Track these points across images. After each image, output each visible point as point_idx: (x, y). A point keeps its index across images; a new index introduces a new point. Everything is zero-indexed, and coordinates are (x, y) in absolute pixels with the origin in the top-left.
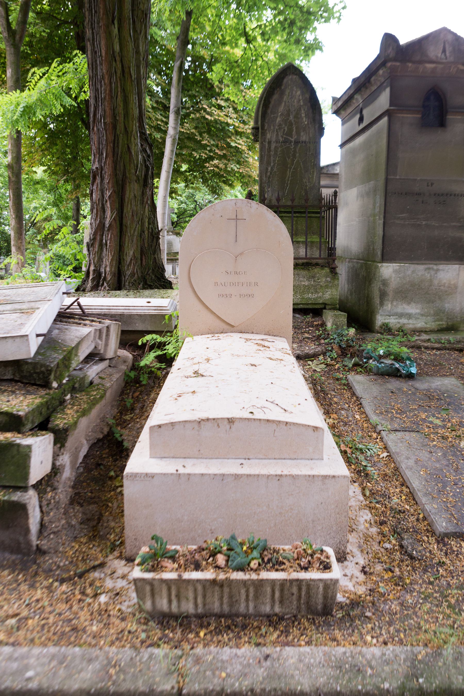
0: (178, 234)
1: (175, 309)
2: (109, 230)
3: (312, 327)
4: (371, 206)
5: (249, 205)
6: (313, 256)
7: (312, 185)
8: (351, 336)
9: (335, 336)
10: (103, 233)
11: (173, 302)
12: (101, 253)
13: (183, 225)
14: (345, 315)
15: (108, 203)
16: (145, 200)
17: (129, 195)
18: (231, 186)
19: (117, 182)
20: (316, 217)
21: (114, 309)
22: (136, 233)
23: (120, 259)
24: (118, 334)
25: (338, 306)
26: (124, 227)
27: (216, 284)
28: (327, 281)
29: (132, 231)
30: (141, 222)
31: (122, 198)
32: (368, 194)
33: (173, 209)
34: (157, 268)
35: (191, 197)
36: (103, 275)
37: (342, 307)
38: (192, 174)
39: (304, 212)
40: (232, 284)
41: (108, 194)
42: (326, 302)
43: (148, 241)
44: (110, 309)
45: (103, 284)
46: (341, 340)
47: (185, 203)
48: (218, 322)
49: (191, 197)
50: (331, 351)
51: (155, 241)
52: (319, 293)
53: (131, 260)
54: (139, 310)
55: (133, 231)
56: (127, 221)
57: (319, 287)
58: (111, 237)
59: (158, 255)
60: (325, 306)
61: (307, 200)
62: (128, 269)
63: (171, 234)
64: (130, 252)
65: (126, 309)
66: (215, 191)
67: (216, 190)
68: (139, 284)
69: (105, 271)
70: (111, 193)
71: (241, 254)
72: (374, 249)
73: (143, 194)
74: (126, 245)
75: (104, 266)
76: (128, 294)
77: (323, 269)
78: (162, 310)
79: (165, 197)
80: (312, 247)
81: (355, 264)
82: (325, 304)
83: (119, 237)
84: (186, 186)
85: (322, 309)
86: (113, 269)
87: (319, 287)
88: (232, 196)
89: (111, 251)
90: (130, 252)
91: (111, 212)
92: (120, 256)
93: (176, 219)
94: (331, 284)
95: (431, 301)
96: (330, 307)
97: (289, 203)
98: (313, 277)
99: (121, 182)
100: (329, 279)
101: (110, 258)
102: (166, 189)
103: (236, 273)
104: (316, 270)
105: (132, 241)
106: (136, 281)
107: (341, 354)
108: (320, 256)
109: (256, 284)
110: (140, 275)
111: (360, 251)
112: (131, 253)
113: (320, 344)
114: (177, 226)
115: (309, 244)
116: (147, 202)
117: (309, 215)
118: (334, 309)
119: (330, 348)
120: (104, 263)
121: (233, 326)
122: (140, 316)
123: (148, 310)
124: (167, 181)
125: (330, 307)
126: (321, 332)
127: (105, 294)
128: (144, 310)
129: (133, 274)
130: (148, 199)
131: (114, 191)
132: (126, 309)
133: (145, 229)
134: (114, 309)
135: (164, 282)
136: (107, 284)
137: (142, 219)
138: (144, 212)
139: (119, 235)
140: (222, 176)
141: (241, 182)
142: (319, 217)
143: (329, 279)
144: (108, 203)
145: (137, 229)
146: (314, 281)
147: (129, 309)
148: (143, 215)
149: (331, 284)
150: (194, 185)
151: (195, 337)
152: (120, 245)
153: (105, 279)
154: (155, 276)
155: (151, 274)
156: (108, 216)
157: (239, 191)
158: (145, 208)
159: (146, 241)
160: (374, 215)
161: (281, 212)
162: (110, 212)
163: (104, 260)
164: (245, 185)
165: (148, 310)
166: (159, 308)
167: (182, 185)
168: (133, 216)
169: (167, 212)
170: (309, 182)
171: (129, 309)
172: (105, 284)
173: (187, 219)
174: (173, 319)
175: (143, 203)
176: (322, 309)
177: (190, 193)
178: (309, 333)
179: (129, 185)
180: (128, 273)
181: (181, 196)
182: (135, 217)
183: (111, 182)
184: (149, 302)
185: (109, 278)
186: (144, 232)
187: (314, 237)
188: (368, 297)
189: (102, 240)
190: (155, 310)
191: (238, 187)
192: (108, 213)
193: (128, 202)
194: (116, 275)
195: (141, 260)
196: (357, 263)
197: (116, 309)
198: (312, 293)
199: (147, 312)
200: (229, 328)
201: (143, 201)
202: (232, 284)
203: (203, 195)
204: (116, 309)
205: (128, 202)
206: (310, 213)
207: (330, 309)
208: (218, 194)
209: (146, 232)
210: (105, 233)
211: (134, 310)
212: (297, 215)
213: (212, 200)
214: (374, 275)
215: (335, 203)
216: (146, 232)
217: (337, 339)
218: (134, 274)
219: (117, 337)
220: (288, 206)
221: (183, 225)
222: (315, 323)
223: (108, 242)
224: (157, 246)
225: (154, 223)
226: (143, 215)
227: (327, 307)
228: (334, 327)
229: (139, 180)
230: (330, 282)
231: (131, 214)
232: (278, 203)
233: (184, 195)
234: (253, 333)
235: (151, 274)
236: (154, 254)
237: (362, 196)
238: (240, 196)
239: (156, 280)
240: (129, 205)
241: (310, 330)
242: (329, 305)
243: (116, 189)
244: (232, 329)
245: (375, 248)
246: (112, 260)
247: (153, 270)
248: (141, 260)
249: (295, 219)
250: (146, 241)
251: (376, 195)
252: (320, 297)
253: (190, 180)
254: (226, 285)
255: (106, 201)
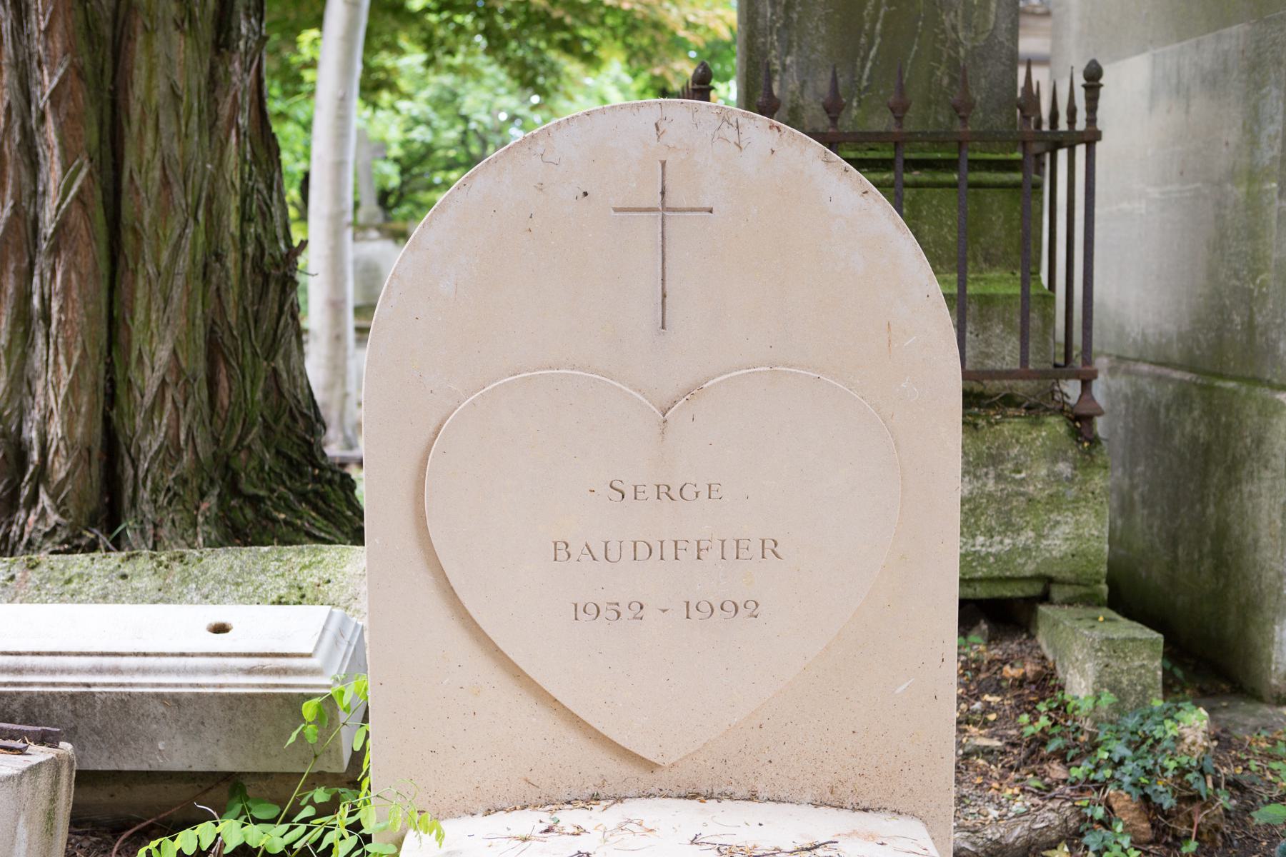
0: (400, 236)
1: (357, 664)
2: (55, 250)
3: (998, 690)
4: (1233, 135)
5: (730, 133)
6: (991, 364)
7: (981, 41)
8: (1198, 751)
9: (1120, 750)
10: (32, 264)
11: (345, 620)
12: (25, 356)
13: (423, 197)
14: (1153, 643)
15: (50, 125)
16: (225, 110)
17: (149, 89)
18: (590, 60)
19: (90, 29)
20: (1003, 186)
21: (42, 671)
22: (183, 263)
23: (112, 383)
24: (50, 816)
25: (1104, 588)
26: (128, 238)
27: (562, 550)
28: (1056, 478)
29: (165, 256)
30: (209, 211)
31: (114, 104)
32: (1213, 81)
33: (383, 146)
34: (285, 418)
35: (446, 101)
36: (35, 456)
37: (1125, 596)
38: (449, 20)
39: (950, 165)
40: (642, 550)
41: (47, 81)
42: (1053, 572)
43: (242, 296)
44: (19, 671)
45: (33, 499)
46: (1149, 773)
47: (428, 123)
48: (574, 747)
49: (446, 101)
50: (1106, 824)
51: (273, 292)
52: (1018, 531)
53: (163, 383)
54: (169, 671)
55: (167, 249)
56: (142, 207)
57: (1018, 502)
58: (66, 281)
59: (287, 358)
60: (1045, 588)
61: (962, 110)
62: (149, 427)
63: (374, 234)
64: (158, 351)
65: (100, 671)
66: (528, 77)
67: (536, 75)
68: (203, 495)
69: (43, 437)
70: (62, 81)
71: (692, 392)
72: (1250, 327)
73: (213, 82)
74: (140, 316)
75: (36, 415)
76: (127, 569)
77: (1037, 423)
78: (284, 671)
79: (343, 101)
80: (984, 320)
81: (1145, 383)
82: (1048, 581)
83: (104, 284)
84: (430, 63)
85: (1031, 603)
86: (79, 430)
87: (1018, 502)
88: (589, 96)
89: (67, 345)
90: (158, 351)
91: (65, 169)
92: (110, 368)
93: (394, 181)
94: (1073, 492)
95: (310, 445)
96: (1068, 591)
97: (881, 122)
98: (995, 459)
99: (107, 31)
100: (1064, 468)
101: (66, 378)
102: (346, 70)
103: (664, 491)
104: (1006, 429)
105: (167, 300)
106: (185, 482)
107: (1149, 836)
108: (1024, 361)
109: (770, 548)
110: (205, 450)
111: (1170, 328)
112: (163, 354)
113: (1045, 792)
114: (394, 206)
115: (972, 309)
116: (232, 120)
117: (973, 177)
118: (1089, 600)
119: (1100, 813)
120: (40, 399)
121: (651, 766)
122: (175, 701)
123: (215, 672)
124: (348, 38)
125: (1068, 591)
126: (1044, 721)
127: (17, 571)
128: (196, 671)
129: (171, 451)
130: (236, 107)
131: (77, 71)
132: (100, 671)
133: (228, 244)
134: (42, 671)
135: (317, 479)
136: (53, 497)
137: (210, 199)
138: (220, 165)
139: (104, 268)
140: (559, 25)
141: (628, 46)
142: (1016, 186)
143: (1064, 468)
144: (50, 125)
145: (186, 244)
146: (999, 478)
147: (116, 671)
148: (213, 182)
149: (1073, 492)
150: (458, 60)
151: (449, 826)
152: (112, 322)
153: (42, 473)
154: (278, 453)
155: (257, 447)
156: (52, 187)
157: (617, 81)
158: (224, 145)
159: (231, 298)
160: (1254, 176)
161: (885, 165)
162: (57, 167)
163: (39, 386)
164: (638, 57)
165: (215, 672)
166: (268, 662)
167: (414, 58)
168: (166, 183)
169: (351, 157)
170: (968, 26)
171: (116, 671)
172: (44, 499)
173: (438, 178)
174: (343, 717)
175: (213, 126)
176: (1031, 603)
177: (444, 88)
178: (986, 723)
179: (148, 44)
180: (152, 444)
181: (409, 97)
182: (177, 189)
183: (59, 26)
184: (220, 629)
185: (60, 469)
186: (219, 257)
187: (994, 274)
188: (1222, 533)
189: (29, 296)
190: (250, 671)
191: (615, 64)
192: (52, 173)
193: (143, 121)
194: (96, 453)
195: (212, 383)
196: (1159, 378)
197: (53, 671)
198: (990, 532)
199: (209, 683)
200: (633, 775)
201: (215, 118)
202: (642, 550)
203: (489, 95)
204: (53, 671)
205: (143, 121)
206: (975, 165)
207: (1070, 602)
208: (542, 91)
209: (231, 259)
210: (42, 262)
211: (145, 671)
212: (916, 175)
213: (523, 111)
214: (1259, 442)
215: (1091, 120)
216: (231, 259)
217: (1129, 766)
218: (179, 451)
219: (50, 831)
220: (879, 137)
221: (423, 197)
222: (1010, 672)
223: (55, 306)
224: (286, 318)
225: (266, 215)
226: (213, 182)
227: (1057, 593)
228: (1108, 698)
229: (192, 21)
230: (1071, 480)
231: (157, 174)
232: (834, 120)
233: (425, 94)
234: (753, 797)
235: (257, 447)
236: (271, 353)
237: (1181, 91)
238: (616, 98)
239: (277, 483)
240: (150, 136)
241: (988, 708)
242: (1063, 582)
243: (85, 60)
244: (646, 780)
245: (1259, 319)
246: (73, 387)
247: (267, 427)
248: (212, 383)
249: (908, 193)
250: (231, 298)
251: (1258, 86)
252: (1026, 549)
253: (442, 42)
254: (613, 555)
255: (42, 118)
